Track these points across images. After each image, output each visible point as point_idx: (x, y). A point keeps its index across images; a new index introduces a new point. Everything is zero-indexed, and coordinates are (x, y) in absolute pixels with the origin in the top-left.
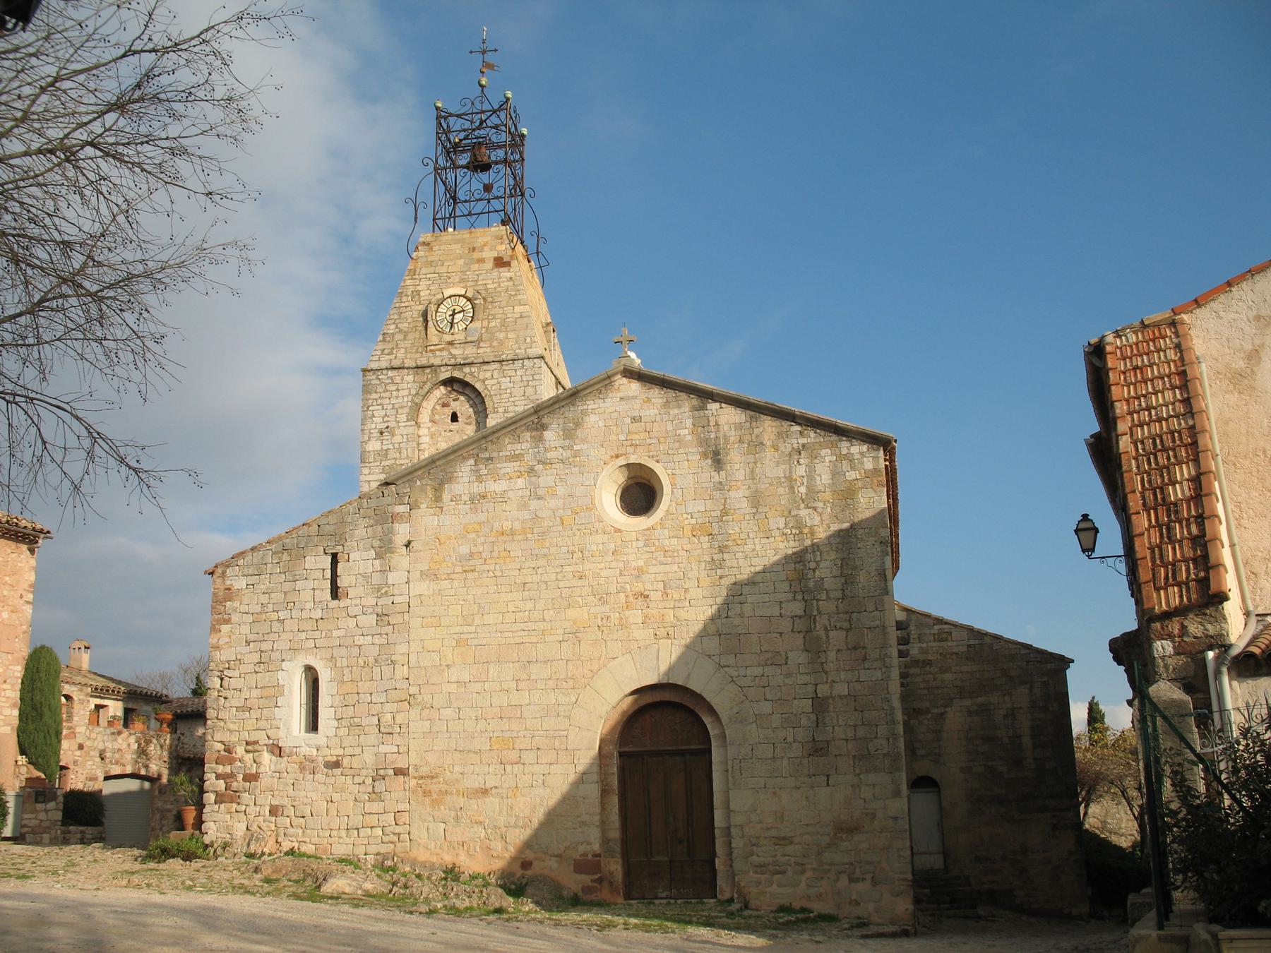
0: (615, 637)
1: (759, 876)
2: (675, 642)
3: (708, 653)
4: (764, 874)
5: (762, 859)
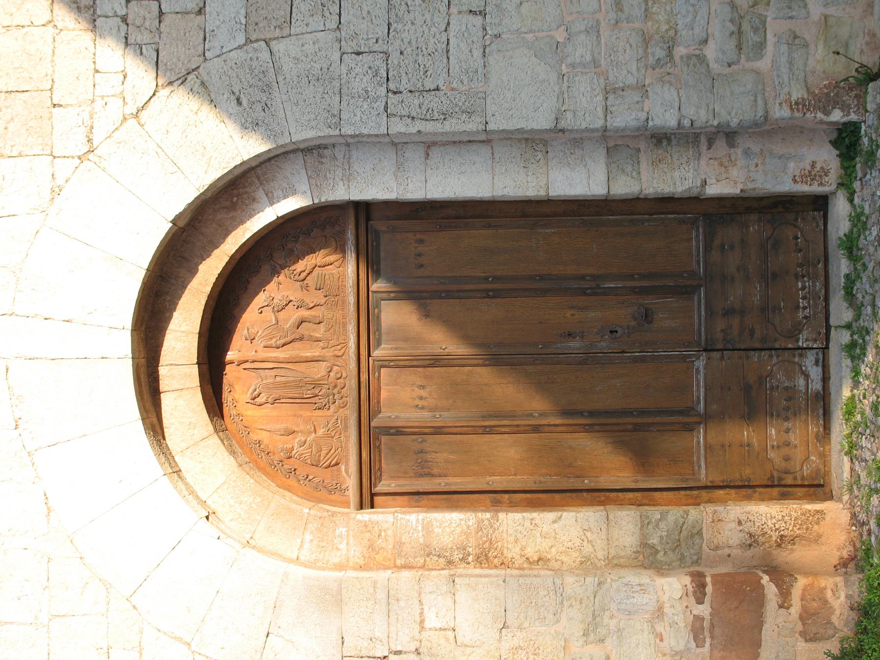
1: (770, 38)
4: (764, 23)
5: (716, 29)
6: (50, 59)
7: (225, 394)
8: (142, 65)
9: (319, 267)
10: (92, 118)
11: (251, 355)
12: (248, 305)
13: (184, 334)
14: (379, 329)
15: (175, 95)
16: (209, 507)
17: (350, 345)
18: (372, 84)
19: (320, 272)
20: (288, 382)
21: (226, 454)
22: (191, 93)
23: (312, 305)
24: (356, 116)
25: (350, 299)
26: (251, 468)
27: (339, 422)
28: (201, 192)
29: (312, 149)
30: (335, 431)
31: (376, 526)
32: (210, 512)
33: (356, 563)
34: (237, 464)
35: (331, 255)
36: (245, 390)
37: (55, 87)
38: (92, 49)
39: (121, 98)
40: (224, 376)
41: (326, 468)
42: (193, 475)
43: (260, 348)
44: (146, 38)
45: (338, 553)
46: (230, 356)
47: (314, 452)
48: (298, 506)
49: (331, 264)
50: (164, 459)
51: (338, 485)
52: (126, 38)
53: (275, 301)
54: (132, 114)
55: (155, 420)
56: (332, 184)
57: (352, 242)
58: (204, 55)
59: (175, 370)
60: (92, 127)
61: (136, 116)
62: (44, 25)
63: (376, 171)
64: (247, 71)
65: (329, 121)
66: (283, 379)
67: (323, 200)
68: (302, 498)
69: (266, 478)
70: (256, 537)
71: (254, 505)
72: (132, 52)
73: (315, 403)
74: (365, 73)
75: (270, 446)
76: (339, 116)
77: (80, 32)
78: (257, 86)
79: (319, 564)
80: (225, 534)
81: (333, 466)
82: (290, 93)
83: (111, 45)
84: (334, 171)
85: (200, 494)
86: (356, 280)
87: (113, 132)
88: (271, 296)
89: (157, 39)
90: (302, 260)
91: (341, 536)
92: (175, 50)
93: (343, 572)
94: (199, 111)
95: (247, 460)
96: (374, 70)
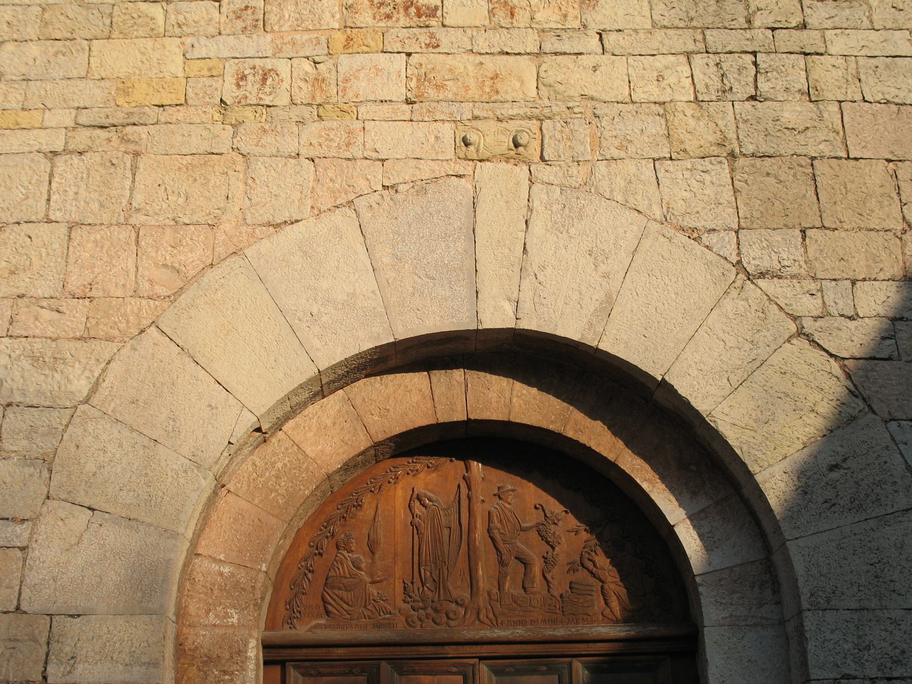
0: (291, 146)
2: (543, 172)
3: (689, 222)
6: (862, 226)
7: (425, 460)
8: (868, 339)
9: (602, 587)
10: (793, 277)
11: (479, 494)
12: (545, 491)
13: (508, 401)
14: (519, 672)
15: (834, 382)
16: (273, 434)
17: (496, 631)
18: (880, 656)
19: (594, 588)
20: (442, 543)
21: (345, 457)
22: (838, 403)
23: (549, 576)
24: (831, 632)
25: (561, 630)
26: (324, 493)
27: (387, 616)
28: (707, 419)
29: (770, 572)
30: (374, 610)
31: (238, 668)
32: (267, 435)
33: (187, 638)
34: (330, 472)
35: (620, 603)
36: (430, 487)
37: (827, 232)
38: (881, 276)
39: (822, 313)
40: (449, 459)
41: (323, 599)
42: (317, 413)
43: (487, 507)
44: (904, 344)
45: (202, 613)
46: (477, 467)
47: (345, 581)
48: (271, 555)
49: (606, 604)
50: (340, 372)
51: (298, 615)
52: (901, 319)
53: (553, 526)
54: (803, 327)
55: (391, 363)
56: (724, 601)
57: (640, 632)
58: (891, 420)
59: (459, 391)
60: (780, 277)
61: (801, 333)
62: (904, 218)
63: (747, 664)
64: (877, 478)
65: (820, 593)
66: (446, 538)
67: (701, 589)
68: (281, 563)
69: (309, 514)
70: (231, 498)
71: (273, 495)
72: (884, 326)
73: (412, 583)
74: (894, 645)
75: (354, 520)
76: (829, 607)
77: (901, 262)
78: (857, 492)
79: (188, 585)
80: (236, 453)
81: (325, 608)
82: (853, 537)
83: (890, 299)
84: (743, 604)
85: (291, 424)
86: (588, 639)
87: (777, 304)
88: (559, 520)
89: (904, 358)
90: (610, 563)
91: (227, 616)
92: (893, 382)
93: (174, 619)
94: (816, 415)
95: (336, 489)
96: (901, 658)
